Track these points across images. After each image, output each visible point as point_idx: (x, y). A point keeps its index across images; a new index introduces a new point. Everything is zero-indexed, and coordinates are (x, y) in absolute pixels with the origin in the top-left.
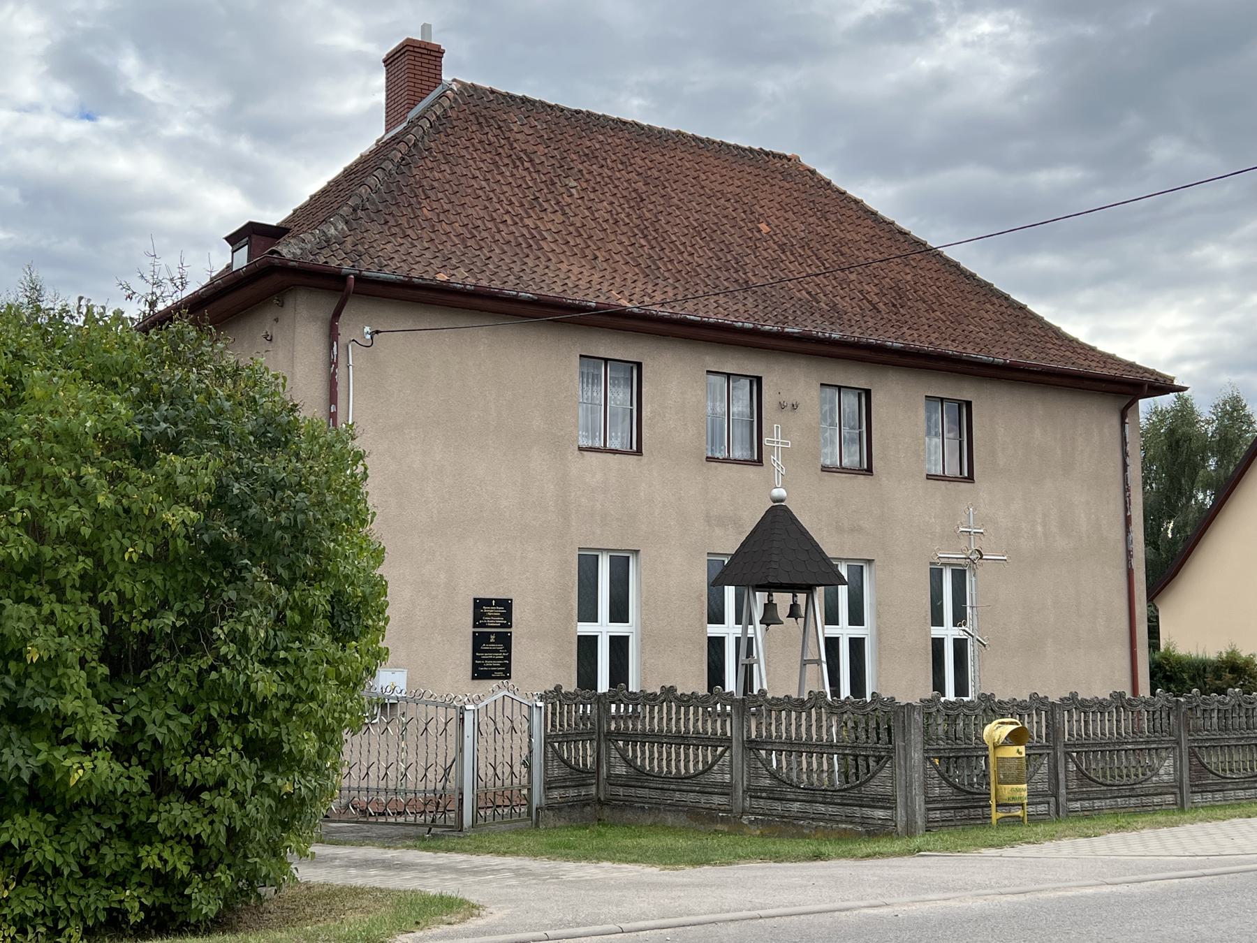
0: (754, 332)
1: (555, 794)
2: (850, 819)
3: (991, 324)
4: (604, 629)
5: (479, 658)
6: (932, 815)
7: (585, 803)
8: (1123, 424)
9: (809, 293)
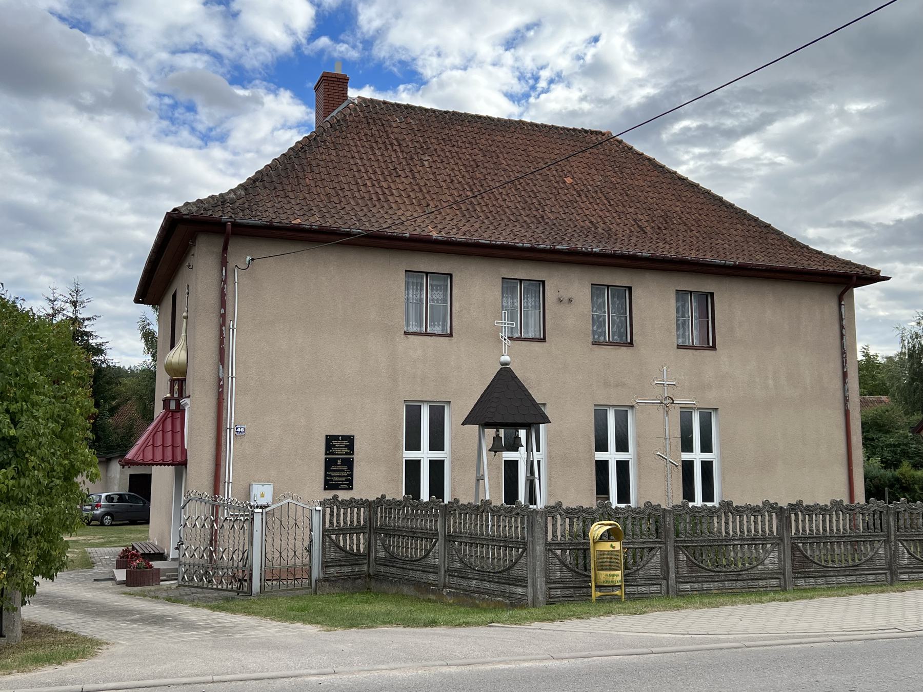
0: (532, 250)
1: (332, 570)
2: (503, 594)
3: (737, 238)
4: (425, 456)
5: (329, 476)
6: (553, 592)
7: (355, 577)
8: (840, 305)
9: (591, 222)
